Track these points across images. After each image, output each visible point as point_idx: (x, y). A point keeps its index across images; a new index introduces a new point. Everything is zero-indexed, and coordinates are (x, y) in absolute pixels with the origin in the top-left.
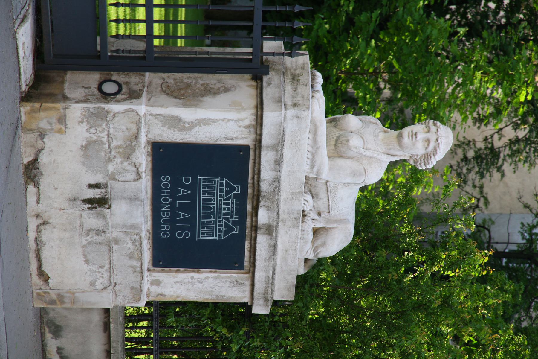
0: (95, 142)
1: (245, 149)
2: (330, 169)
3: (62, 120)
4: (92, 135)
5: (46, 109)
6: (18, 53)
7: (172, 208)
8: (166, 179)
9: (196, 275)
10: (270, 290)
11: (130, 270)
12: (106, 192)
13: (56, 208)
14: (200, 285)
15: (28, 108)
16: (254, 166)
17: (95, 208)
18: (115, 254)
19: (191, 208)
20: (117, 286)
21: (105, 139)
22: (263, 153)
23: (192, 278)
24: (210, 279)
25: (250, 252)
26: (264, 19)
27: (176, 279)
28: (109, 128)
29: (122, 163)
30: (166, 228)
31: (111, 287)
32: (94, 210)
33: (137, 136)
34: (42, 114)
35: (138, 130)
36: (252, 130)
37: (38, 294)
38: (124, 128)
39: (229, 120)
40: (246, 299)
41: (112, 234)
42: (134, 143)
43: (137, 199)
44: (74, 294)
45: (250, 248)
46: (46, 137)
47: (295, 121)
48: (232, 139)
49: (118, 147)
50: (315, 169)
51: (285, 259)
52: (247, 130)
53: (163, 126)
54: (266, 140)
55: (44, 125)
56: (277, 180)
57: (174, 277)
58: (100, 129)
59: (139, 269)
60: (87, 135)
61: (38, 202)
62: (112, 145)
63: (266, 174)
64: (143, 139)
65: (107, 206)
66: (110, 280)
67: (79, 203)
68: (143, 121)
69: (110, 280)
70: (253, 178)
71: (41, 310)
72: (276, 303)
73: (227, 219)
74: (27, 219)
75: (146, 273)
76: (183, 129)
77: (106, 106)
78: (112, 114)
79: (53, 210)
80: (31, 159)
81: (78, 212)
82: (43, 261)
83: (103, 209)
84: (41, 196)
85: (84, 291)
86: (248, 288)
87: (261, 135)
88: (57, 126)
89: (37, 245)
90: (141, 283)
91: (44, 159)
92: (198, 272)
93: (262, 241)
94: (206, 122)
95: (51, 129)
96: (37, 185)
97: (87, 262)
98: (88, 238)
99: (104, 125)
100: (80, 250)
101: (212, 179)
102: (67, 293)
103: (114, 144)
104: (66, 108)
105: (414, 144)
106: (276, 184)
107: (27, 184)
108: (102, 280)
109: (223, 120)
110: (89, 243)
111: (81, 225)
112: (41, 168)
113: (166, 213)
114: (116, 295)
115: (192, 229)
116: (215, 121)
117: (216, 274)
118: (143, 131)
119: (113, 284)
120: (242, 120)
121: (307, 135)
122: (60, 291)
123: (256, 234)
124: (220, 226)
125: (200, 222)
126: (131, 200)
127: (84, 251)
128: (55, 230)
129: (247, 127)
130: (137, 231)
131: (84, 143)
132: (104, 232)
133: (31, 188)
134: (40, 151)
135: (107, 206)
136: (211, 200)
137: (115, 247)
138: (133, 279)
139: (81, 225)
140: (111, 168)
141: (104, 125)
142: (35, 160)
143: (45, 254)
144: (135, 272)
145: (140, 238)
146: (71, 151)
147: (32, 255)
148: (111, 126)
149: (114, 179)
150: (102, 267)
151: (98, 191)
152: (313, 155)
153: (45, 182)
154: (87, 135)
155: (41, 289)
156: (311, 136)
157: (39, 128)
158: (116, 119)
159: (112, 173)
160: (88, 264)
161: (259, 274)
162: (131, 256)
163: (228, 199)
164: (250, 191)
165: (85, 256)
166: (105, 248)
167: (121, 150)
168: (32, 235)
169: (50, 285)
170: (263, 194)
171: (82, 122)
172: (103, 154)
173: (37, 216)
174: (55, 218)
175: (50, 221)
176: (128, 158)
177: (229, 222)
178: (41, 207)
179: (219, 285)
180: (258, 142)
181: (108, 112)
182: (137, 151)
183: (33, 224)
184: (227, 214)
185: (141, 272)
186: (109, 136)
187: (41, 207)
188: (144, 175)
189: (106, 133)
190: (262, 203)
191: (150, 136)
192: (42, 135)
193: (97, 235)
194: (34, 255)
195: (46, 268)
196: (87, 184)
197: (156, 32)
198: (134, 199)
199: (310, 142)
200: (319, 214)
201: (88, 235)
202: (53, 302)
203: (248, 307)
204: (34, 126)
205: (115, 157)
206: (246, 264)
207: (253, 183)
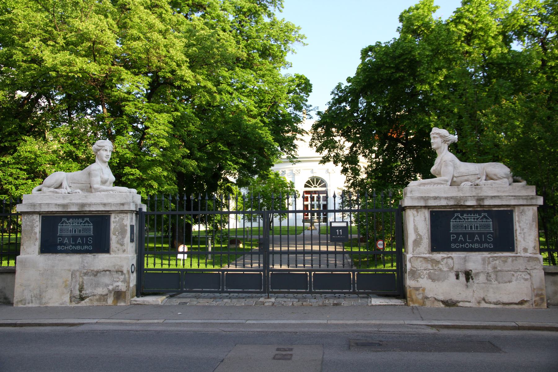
0: (429, 276)
1: (432, 213)
2: (444, 176)
3: (417, 289)
4: (425, 277)
5: (411, 295)
6: (385, 305)
7: (75, 245)
8: (453, 246)
9: (518, 232)
10: (524, 197)
11: (515, 262)
12: (461, 272)
13: (473, 294)
14: (525, 230)
15: (410, 303)
16: (441, 208)
17: (472, 277)
18: (504, 269)
19: (472, 235)
20: (528, 268)
21: (428, 272)
22: (430, 205)
23: (520, 233)
24: (520, 225)
25: (500, 208)
26: (190, 210)
27: (522, 241)
28: (421, 270)
29: (442, 265)
30: (485, 245)
31: (528, 271)
32: (473, 277)
33: (425, 258)
34: (414, 297)
35: (421, 257)
36: (419, 210)
37: (536, 306)
38: (420, 263)
39: (414, 220)
40: (535, 208)
41: (489, 269)
42: (429, 259)
43: (465, 258)
44: (534, 289)
45: (497, 207)
46: (427, 296)
47: (413, 193)
48: (425, 218)
49: (432, 266)
50: (443, 182)
51: (504, 192)
52: (419, 212)
53: (420, 247)
54: (422, 204)
55: (420, 297)
56: (446, 198)
57: (520, 242)
58: (422, 274)
59: (514, 258)
60: (425, 279)
61: (470, 302)
62: (431, 268)
63: (443, 203)
64: (427, 255)
65: (470, 272)
66: (523, 272)
67: (469, 284)
68: (415, 255)
69: (523, 272)
70: (450, 208)
71: (548, 305)
72: (537, 194)
73: (81, 223)
74: (482, 308)
75: (519, 255)
76: (421, 238)
77: (408, 270)
78: (413, 268)
79: (475, 296)
80: (441, 303)
81: (475, 285)
82: (511, 302)
83: (472, 273)
84: (466, 300)
85: (532, 284)
86: (526, 208)
87: (421, 206)
88: (421, 291)
89: (499, 304)
90: (525, 257)
91: (441, 298)
92: (516, 230)
93: (487, 203)
94: (416, 230)
95: (423, 294)
96: (459, 302)
97: (510, 282)
98: (493, 281)
99: (419, 272)
100: (502, 285)
101: (451, 226)
102: (534, 292)
103: (430, 267)
104: (410, 287)
105: (436, 143)
106: (449, 198)
107: (457, 306)
108: (523, 275)
109: (414, 222)
110: (496, 280)
111: (484, 283)
112: (447, 299)
113: (476, 246)
114: (535, 269)
115: (87, 237)
116: (415, 226)
117: (517, 222)
118: (423, 255)
119: (526, 270)
120: (414, 214)
121: (426, 187)
122: (533, 295)
123: (486, 205)
124: (85, 225)
125: (85, 234)
126: (465, 261)
127: (502, 283)
128: (488, 295)
129: (418, 212)
130: (487, 259)
131: (430, 280)
132: (488, 273)
133: (461, 304)
134: (435, 299)
135: (470, 272)
136: (70, 230)
137: (499, 268)
138: (521, 261)
139: (484, 283)
140: (445, 269)
141: (419, 272)
142: (443, 302)
143: (506, 300)
144: (516, 260)
145: (491, 257)
146: (436, 286)
147: (507, 307)
148: (419, 269)
149: (453, 268)
150: (513, 275)
151: (460, 275)
152: (435, 184)
153: (455, 298)
154: (425, 279)
155: (532, 304)
156: (426, 186)
157: (422, 299)
158: (415, 266)
159: (449, 268)
160: (511, 281)
161: (513, 202)
162: (505, 262)
163: (464, 219)
164: (459, 209)
165: (506, 282)
166: (499, 273)
167: (434, 265)
168: (492, 306)
169: (528, 299)
170: (456, 203)
171: (418, 281)
172: (436, 273)
173: (479, 303)
174: (480, 294)
175: (482, 297)
176: (439, 262)
177: (479, 218)
178: (473, 300)
179: (524, 221)
180: (426, 207)
181: (411, 270)
182: (434, 258)
183: (484, 305)
184: (474, 219)
185: (516, 257)
186: (425, 270)
187: (473, 300)
188: (450, 255)
189: (423, 271)
190: (462, 204)
191: (426, 252)
192: (427, 298)
193: (490, 276)
194: (507, 306)
195: (517, 301)
196: (456, 280)
197: (278, 249)
198: (465, 260)
199: (429, 186)
200: (479, 178)
201: (491, 281)
202: (542, 299)
203: (540, 208)
204: (422, 301)
205: (439, 267)
206: (509, 209)
207: (454, 208)
